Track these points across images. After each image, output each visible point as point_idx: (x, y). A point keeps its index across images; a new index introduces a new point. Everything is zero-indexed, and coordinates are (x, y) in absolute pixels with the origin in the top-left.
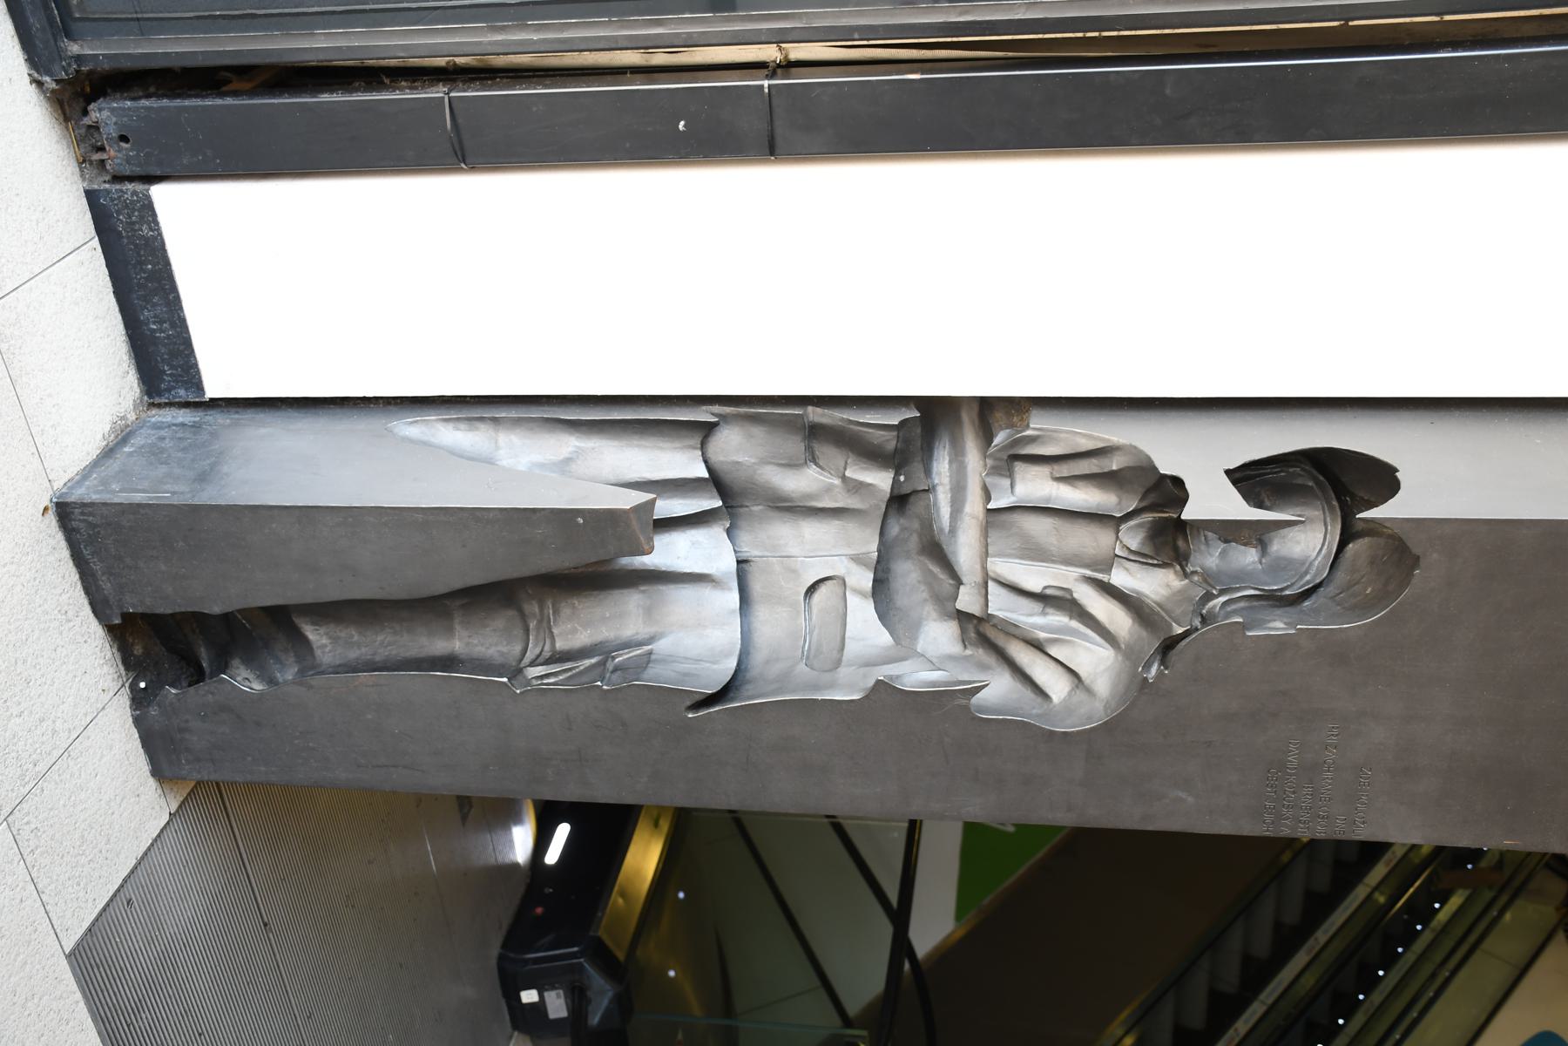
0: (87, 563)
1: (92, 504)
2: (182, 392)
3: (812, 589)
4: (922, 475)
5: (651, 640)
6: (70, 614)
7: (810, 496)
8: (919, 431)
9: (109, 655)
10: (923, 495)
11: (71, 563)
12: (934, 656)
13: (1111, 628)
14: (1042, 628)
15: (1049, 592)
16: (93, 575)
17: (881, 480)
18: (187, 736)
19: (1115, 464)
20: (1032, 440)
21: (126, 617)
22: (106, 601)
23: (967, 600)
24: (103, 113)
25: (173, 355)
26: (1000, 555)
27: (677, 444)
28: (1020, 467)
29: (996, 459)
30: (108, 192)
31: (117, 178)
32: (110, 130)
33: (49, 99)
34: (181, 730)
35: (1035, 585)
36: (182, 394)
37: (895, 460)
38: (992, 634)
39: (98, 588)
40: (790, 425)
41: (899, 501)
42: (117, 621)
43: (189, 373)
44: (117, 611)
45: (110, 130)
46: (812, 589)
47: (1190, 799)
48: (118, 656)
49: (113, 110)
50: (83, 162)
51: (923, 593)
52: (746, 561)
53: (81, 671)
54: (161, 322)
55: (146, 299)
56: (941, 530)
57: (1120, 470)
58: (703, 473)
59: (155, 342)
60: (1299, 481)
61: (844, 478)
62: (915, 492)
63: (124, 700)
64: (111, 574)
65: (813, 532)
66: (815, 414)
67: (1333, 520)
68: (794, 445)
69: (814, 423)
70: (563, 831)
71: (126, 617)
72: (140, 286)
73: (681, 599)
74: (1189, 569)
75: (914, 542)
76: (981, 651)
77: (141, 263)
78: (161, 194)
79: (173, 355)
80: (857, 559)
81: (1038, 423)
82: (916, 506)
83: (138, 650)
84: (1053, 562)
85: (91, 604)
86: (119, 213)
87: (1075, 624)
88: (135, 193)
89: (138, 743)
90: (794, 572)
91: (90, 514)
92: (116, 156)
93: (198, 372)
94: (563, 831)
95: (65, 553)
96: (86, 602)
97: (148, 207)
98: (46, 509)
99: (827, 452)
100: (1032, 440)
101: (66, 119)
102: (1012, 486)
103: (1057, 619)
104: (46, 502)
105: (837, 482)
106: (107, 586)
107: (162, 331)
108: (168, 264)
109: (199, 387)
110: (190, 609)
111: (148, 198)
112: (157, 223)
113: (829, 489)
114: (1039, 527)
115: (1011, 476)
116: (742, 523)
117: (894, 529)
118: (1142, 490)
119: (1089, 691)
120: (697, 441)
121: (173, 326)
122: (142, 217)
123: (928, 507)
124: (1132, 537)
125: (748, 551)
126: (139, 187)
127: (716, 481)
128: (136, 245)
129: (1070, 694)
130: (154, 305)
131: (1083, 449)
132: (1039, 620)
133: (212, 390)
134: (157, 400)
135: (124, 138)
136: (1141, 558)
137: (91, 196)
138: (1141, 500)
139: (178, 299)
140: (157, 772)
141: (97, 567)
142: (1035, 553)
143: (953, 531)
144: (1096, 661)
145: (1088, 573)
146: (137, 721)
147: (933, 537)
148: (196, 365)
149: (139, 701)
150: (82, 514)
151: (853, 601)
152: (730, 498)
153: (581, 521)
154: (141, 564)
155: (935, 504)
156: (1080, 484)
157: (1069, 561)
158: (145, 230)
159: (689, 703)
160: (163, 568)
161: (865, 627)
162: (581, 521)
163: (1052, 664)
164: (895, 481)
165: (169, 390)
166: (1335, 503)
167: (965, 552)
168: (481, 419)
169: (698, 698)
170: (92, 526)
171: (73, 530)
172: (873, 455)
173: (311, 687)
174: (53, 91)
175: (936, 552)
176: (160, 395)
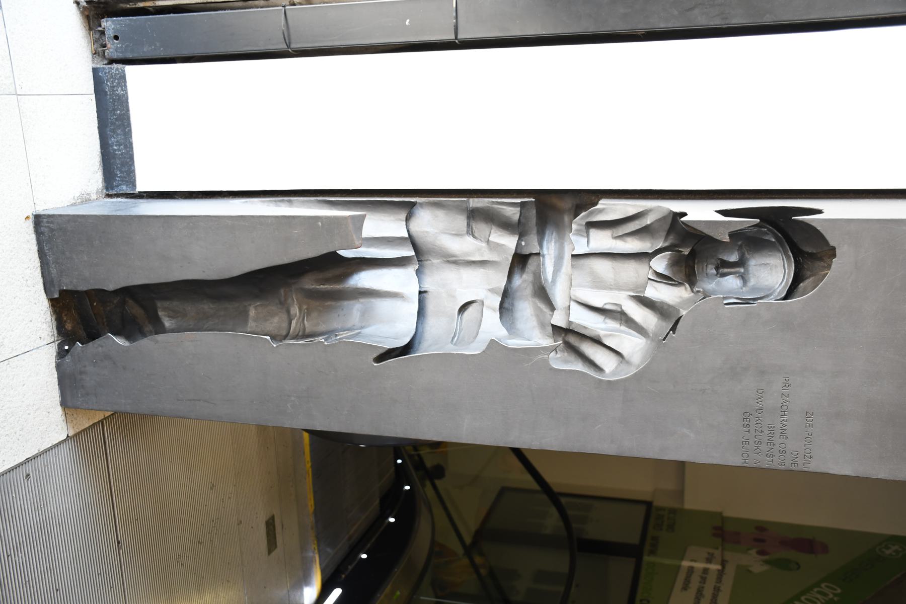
0: (46, 255)
1: (53, 216)
2: (124, 187)
3: (464, 308)
4: (536, 244)
5: (362, 328)
6: (29, 282)
7: (468, 254)
8: (534, 212)
9: (49, 319)
10: (535, 257)
11: (36, 255)
12: (531, 334)
13: (644, 326)
14: (602, 329)
15: (608, 307)
16: (48, 264)
17: (509, 242)
18: (84, 377)
19: (648, 220)
20: (600, 211)
21: (62, 292)
22: (52, 282)
23: (558, 320)
24: (109, 24)
25: (123, 164)
26: (580, 286)
27: (392, 218)
28: (593, 232)
29: (579, 225)
30: (104, 69)
31: (112, 61)
32: (110, 33)
33: (82, 13)
34: (81, 373)
35: (599, 304)
36: (124, 189)
37: (517, 228)
38: (572, 340)
39: (49, 272)
40: (459, 209)
41: (520, 260)
42: (56, 296)
43: (130, 177)
44: (57, 289)
45: (110, 33)
46: (464, 308)
47: (692, 435)
48: (55, 323)
49: (113, 21)
50: (95, 53)
51: (533, 322)
52: (425, 292)
53: (31, 321)
54: (120, 145)
55: (114, 131)
56: (546, 280)
57: (652, 224)
58: (407, 236)
59: (114, 156)
60: (767, 238)
61: (488, 242)
62: (531, 255)
63: (53, 350)
64: (57, 263)
65: (468, 274)
66: (476, 203)
67: (789, 266)
68: (461, 221)
69: (473, 205)
70: (337, 592)
71: (62, 292)
72: (112, 123)
73: (383, 306)
74: (696, 289)
75: (529, 291)
76: (566, 354)
77: (114, 110)
78: (131, 71)
79: (123, 164)
80: (492, 291)
81: (603, 203)
82: (532, 264)
83: (69, 326)
84: (611, 289)
85: (44, 284)
86: (107, 80)
87: (623, 328)
88: (117, 69)
89: (56, 381)
90: (453, 297)
91: (52, 222)
92: (113, 49)
93: (135, 176)
94: (337, 592)
95: (35, 248)
96: (41, 281)
97: (123, 77)
98: (28, 217)
99: (481, 228)
100: (600, 211)
101: (90, 29)
102: (588, 242)
103: (612, 324)
104: (30, 214)
105: (484, 245)
106: (54, 271)
107: (119, 150)
108: (128, 110)
109: (133, 184)
110: (100, 304)
111: (124, 71)
112: (125, 86)
113: (479, 250)
114: (603, 267)
115: (588, 236)
116: (427, 271)
117: (518, 281)
118: (664, 234)
119: (628, 363)
120: (403, 216)
121: (126, 147)
122: (119, 83)
123: (539, 265)
124: (660, 264)
125: (426, 286)
126: (120, 66)
127: (412, 240)
128: (114, 100)
129: (616, 368)
130: (118, 135)
131: (631, 214)
132: (603, 326)
133: (141, 187)
134: (111, 192)
135: (116, 38)
136: (663, 278)
137: (95, 71)
138: (666, 240)
139: (130, 131)
140: (64, 404)
141: (50, 259)
142: (599, 284)
143: (554, 281)
144: (632, 345)
145: (632, 294)
146: (58, 367)
147: (541, 282)
148: (134, 171)
149: (61, 354)
150: (48, 222)
151: (487, 312)
152: (419, 254)
153: (320, 224)
154: (74, 257)
155: (543, 264)
156: (629, 239)
157: (618, 287)
158: (120, 92)
159: (375, 355)
160: (86, 258)
161: (491, 326)
162: (320, 224)
163: (607, 352)
164: (518, 245)
165: (117, 186)
166: (790, 254)
167: (559, 295)
168: (282, 201)
169: (382, 351)
170: (52, 230)
171: (42, 233)
172: (506, 225)
173: (157, 342)
174: (84, 7)
175: (542, 294)
176: (112, 189)
